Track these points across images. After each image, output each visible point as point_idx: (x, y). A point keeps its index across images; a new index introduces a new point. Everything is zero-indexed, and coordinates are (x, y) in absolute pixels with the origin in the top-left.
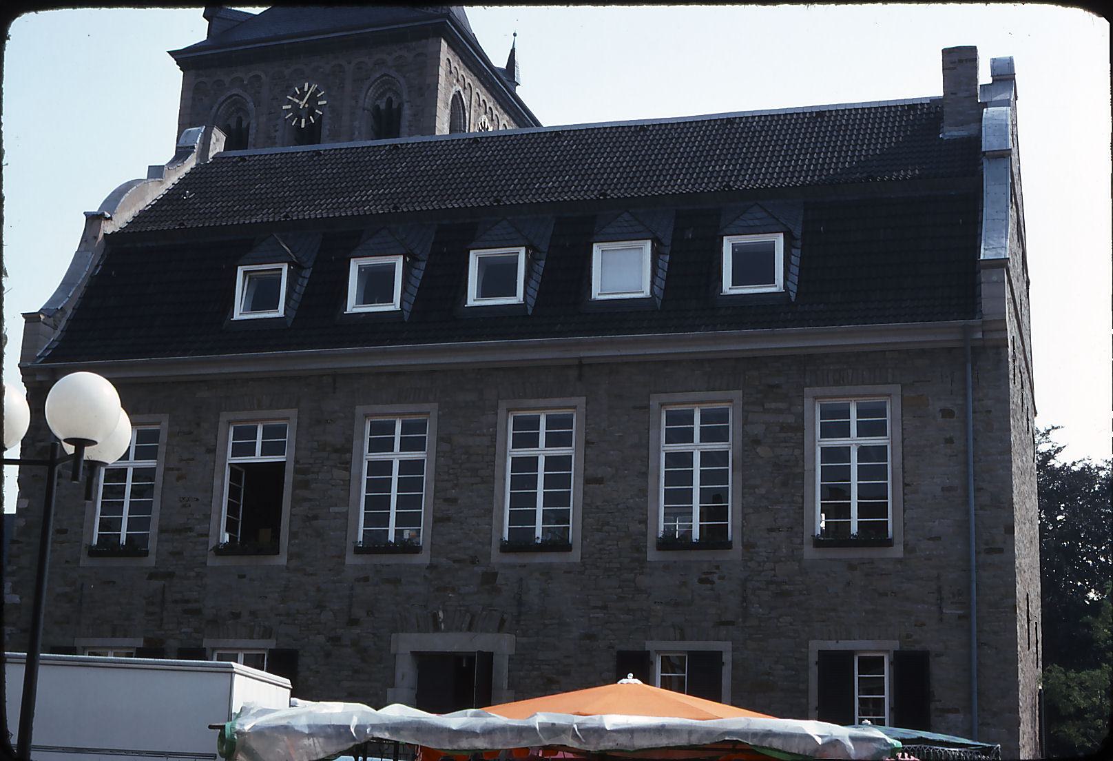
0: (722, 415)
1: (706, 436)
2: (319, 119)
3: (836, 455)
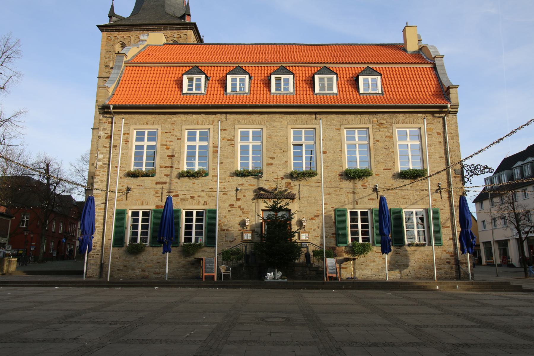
0: (155, 133)
1: (201, 139)
3: (352, 148)
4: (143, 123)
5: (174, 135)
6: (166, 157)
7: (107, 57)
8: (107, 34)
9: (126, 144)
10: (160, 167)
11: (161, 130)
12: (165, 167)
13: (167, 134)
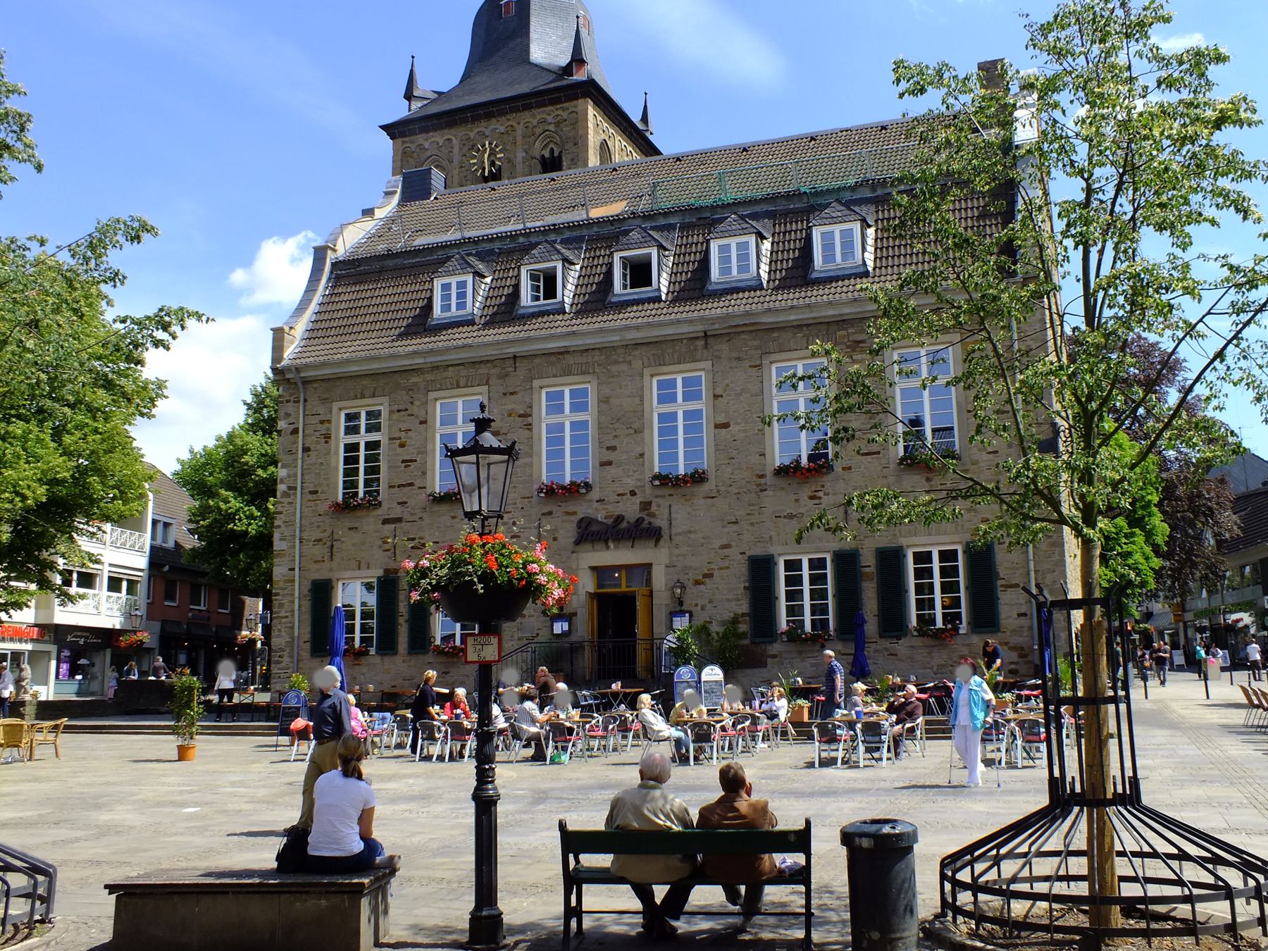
0: (697, 381)
2: (500, 168)
3: (668, 418)
9: (326, 442)
10: (390, 487)
12: (399, 486)
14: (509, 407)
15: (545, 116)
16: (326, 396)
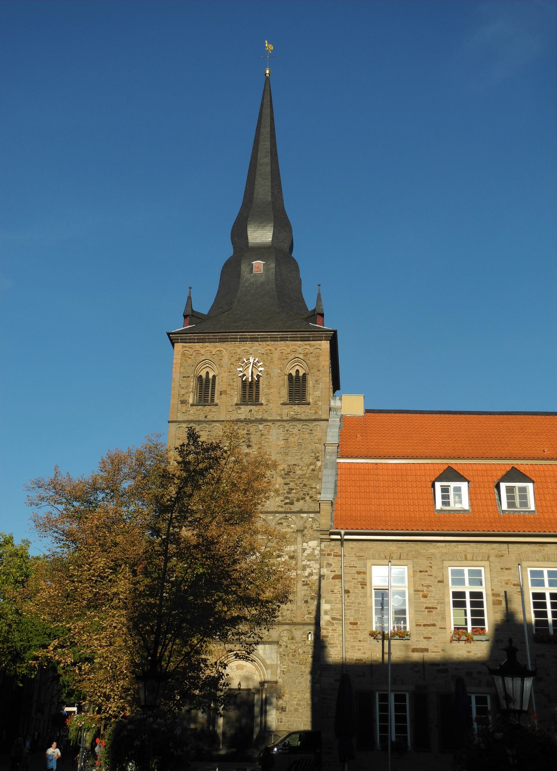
4: (385, 557)
5: (432, 576)
6: (424, 609)
7: (184, 385)
8: (184, 347)
9: (363, 588)
10: (417, 625)
11: (413, 567)
12: (424, 625)
13: (423, 573)
14: (506, 578)
15: (296, 348)
16: (361, 554)
